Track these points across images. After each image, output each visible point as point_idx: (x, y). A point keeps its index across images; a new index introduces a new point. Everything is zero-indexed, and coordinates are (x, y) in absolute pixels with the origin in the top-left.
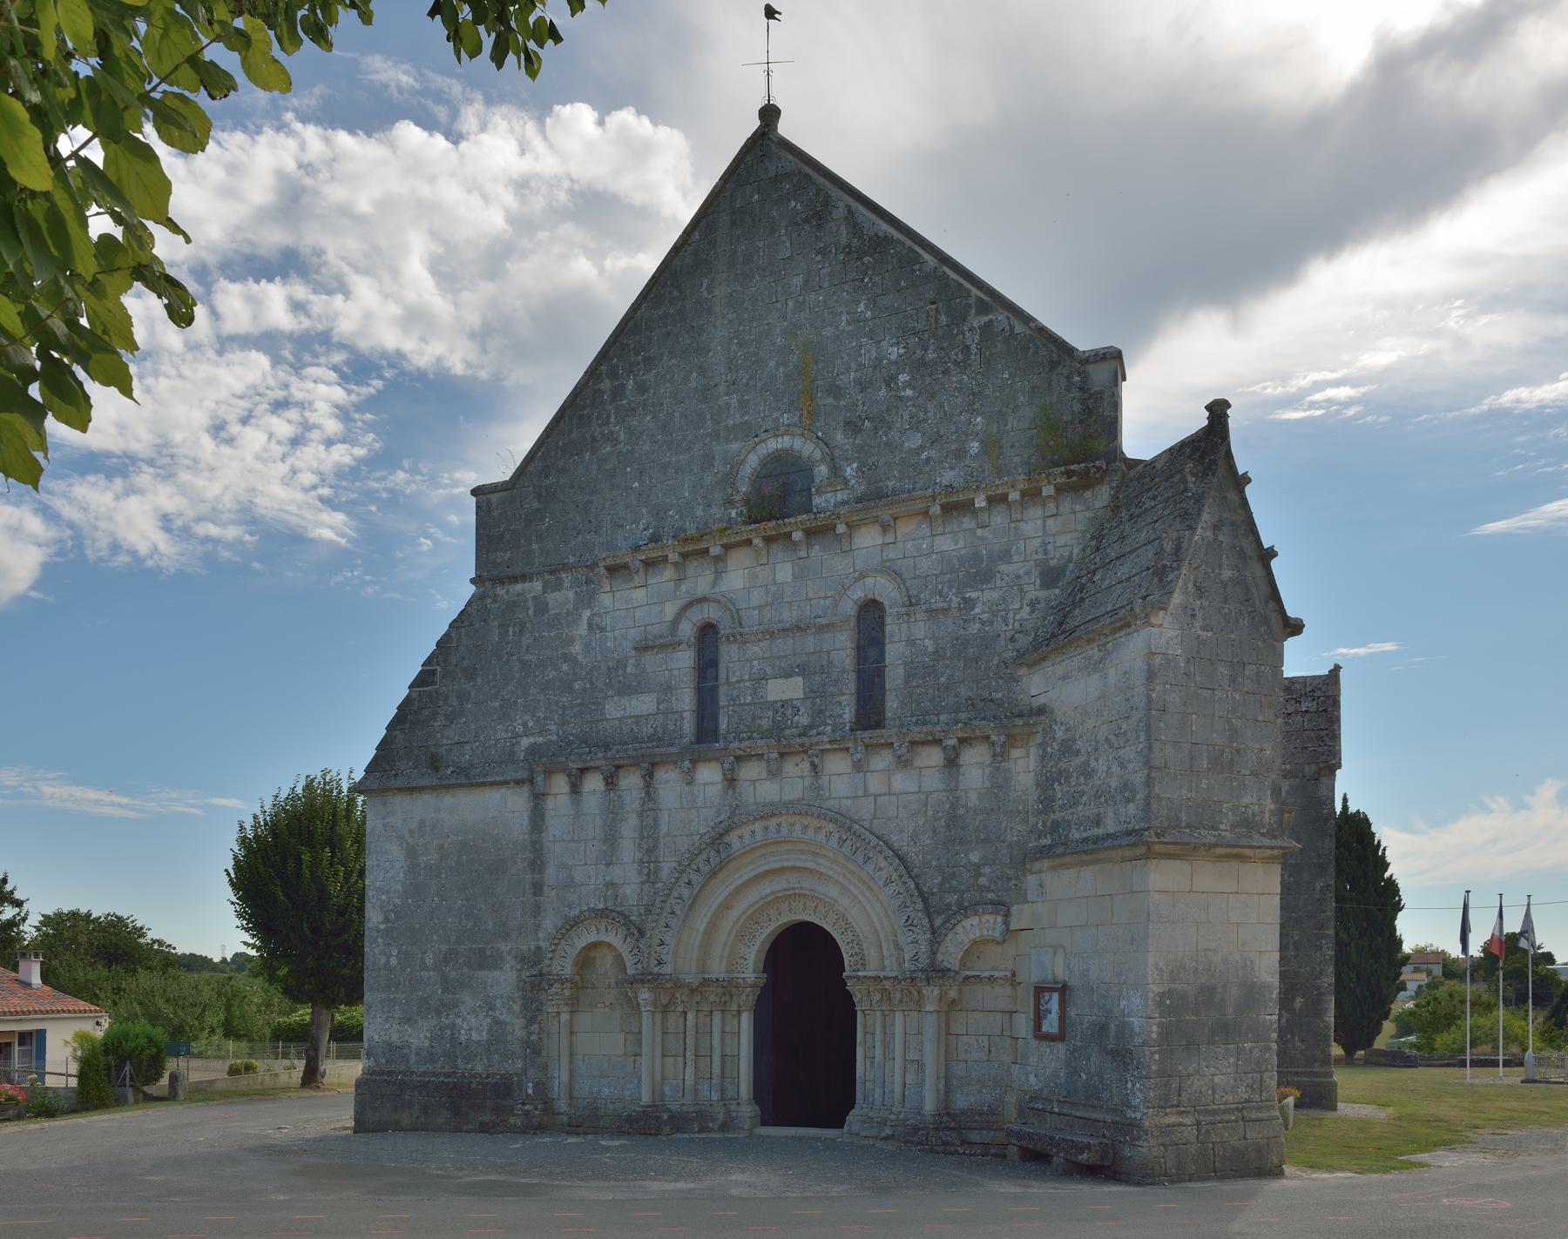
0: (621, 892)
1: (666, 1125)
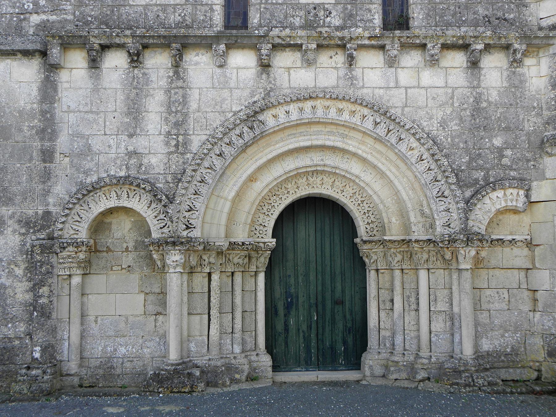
0: (145, 161)
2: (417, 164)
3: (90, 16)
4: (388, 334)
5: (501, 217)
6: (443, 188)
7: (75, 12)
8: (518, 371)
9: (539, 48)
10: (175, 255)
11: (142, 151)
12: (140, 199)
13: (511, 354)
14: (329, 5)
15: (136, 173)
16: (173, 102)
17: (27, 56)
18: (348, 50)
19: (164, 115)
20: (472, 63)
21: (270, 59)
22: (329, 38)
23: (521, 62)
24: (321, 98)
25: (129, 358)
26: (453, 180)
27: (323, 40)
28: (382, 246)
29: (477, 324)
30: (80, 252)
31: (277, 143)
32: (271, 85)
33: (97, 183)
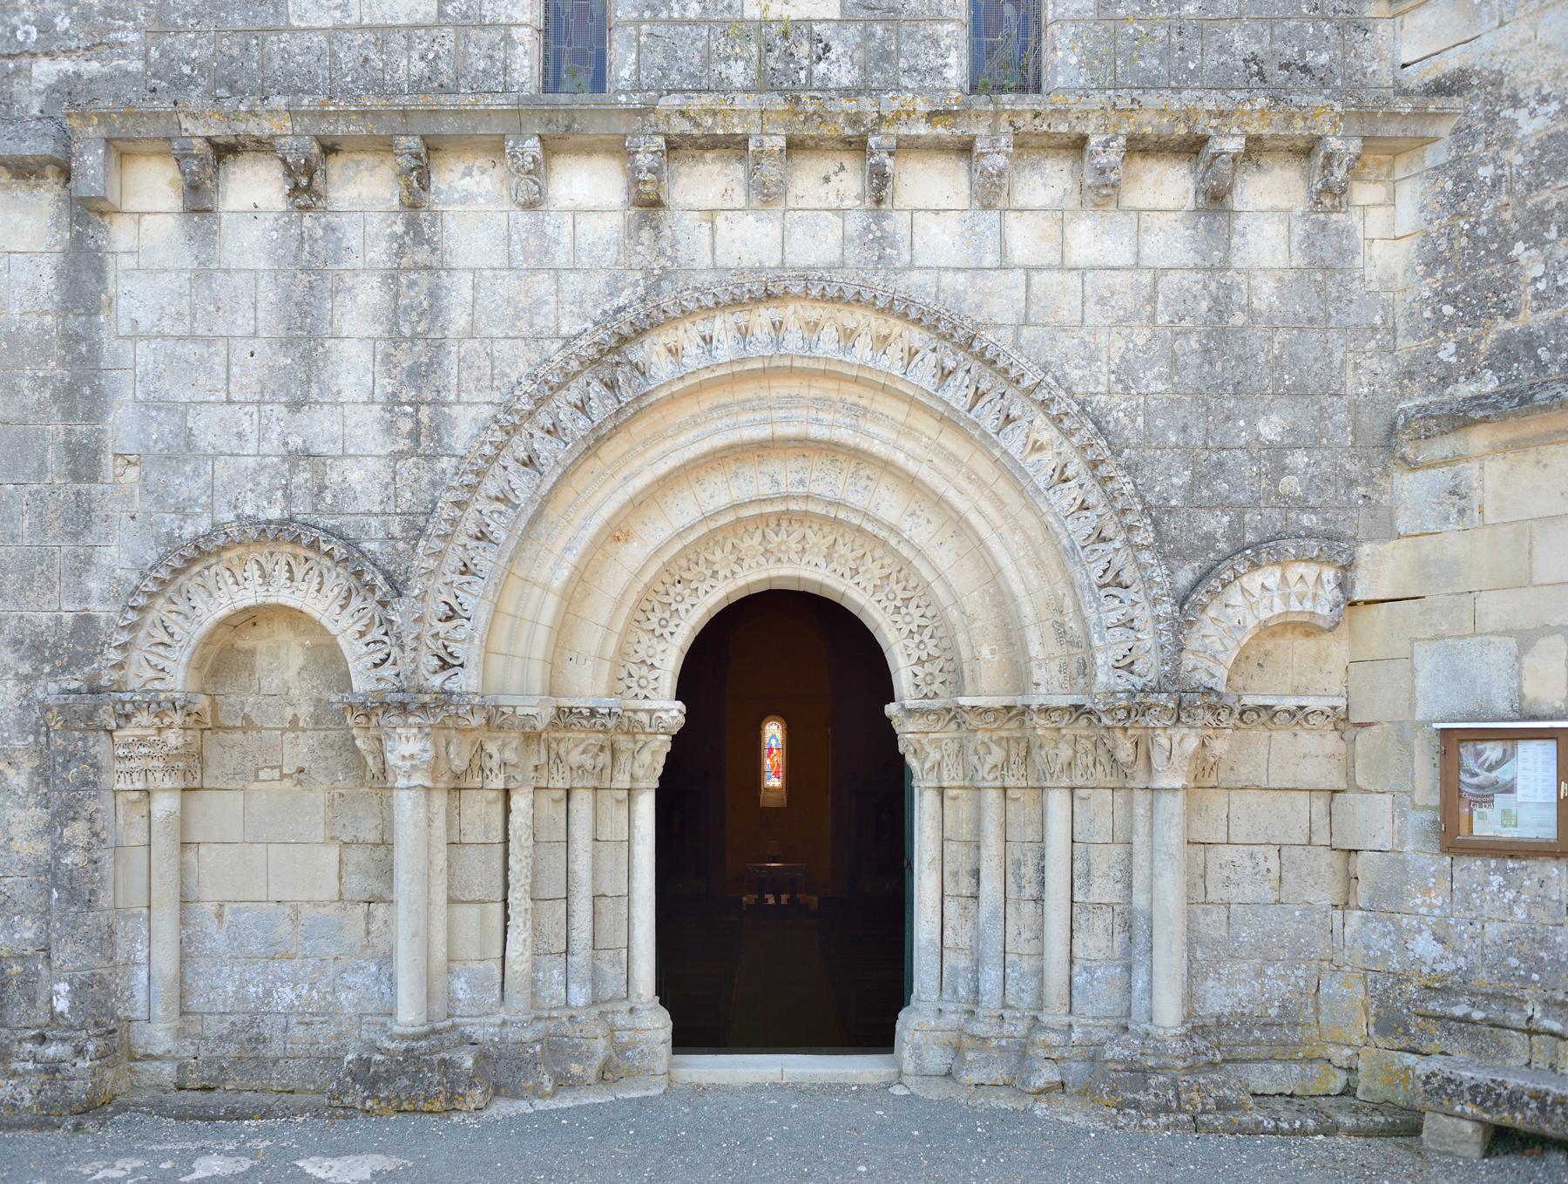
0: (333, 477)
1: (472, 1085)
2: (1051, 491)
3: (187, 63)
4: (963, 962)
5: (1268, 645)
6: (1119, 561)
7: (148, 51)
8: (1296, 1069)
9: (1395, 153)
10: (408, 739)
11: (323, 449)
12: (321, 584)
13: (1280, 1025)
14: (824, 25)
15: (309, 510)
16: (405, 309)
17: (24, 177)
18: (872, 154)
19: (381, 346)
20: (1209, 195)
21: (660, 181)
22: (820, 116)
23: (1344, 191)
24: (796, 297)
25: (300, 1014)
26: (1145, 536)
27: (804, 123)
28: (953, 725)
29: (1193, 941)
30: (170, 727)
31: (681, 428)
32: (663, 261)
33: (207, 537)
